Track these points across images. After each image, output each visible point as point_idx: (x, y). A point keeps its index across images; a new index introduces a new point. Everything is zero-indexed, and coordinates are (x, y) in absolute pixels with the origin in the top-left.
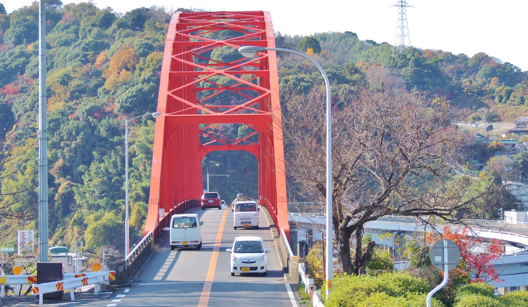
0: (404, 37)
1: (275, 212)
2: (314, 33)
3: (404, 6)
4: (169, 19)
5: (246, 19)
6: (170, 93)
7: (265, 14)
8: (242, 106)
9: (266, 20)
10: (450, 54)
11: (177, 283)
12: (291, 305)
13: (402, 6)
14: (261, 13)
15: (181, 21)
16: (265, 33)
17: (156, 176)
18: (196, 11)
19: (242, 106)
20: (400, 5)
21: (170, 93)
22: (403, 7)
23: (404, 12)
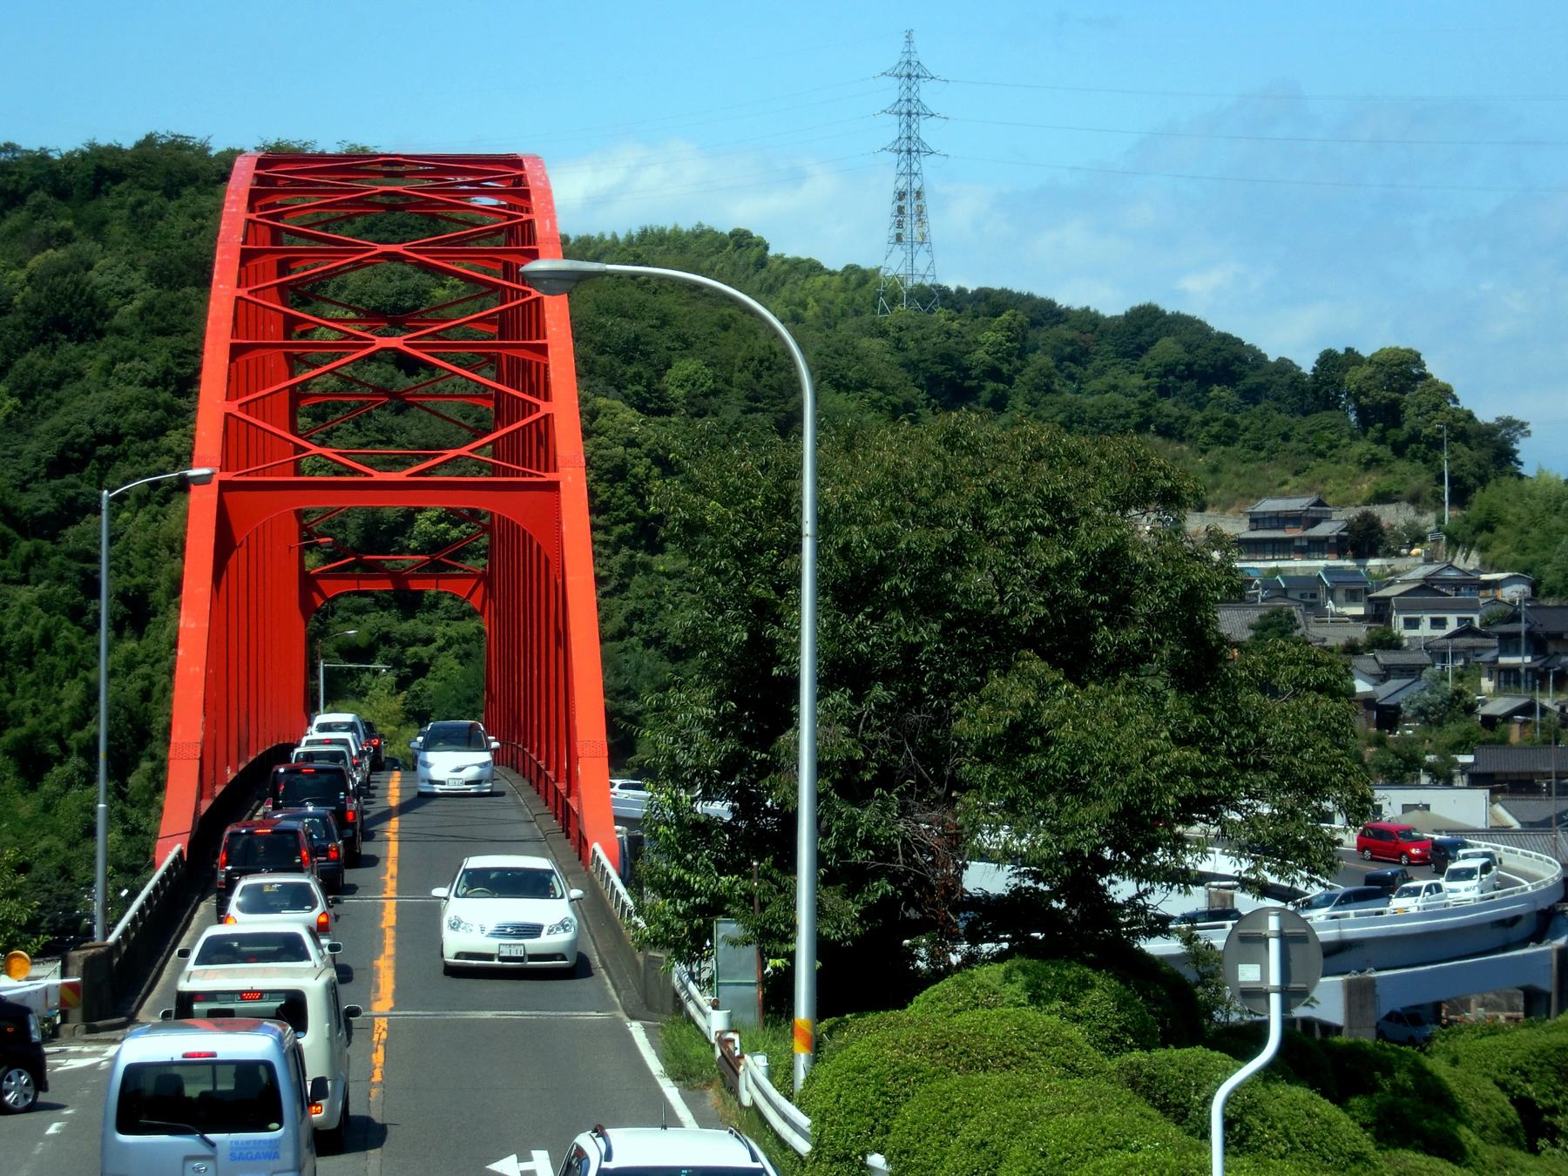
0: (916, 247)
1: (562, 786)
2: (626, 232)
3: (918, 151)
4: (224, 168)
5: (469, 179)
6: (545, 408)
7: (526, 165)
8: (464, 451)
9: (532, 183)
10: (1051, 304)
11: (144, 990)
12: (1206, 1169)
13: (909, 151)
14: (515, 162)
15: (260, 179)
16: (530, 222)
17: (192, 670)
18: (296, 146)
19: (464, 451)
20: (904, 148)
21: (233, 407)
22: (914, 154)
23: (915, 167)
